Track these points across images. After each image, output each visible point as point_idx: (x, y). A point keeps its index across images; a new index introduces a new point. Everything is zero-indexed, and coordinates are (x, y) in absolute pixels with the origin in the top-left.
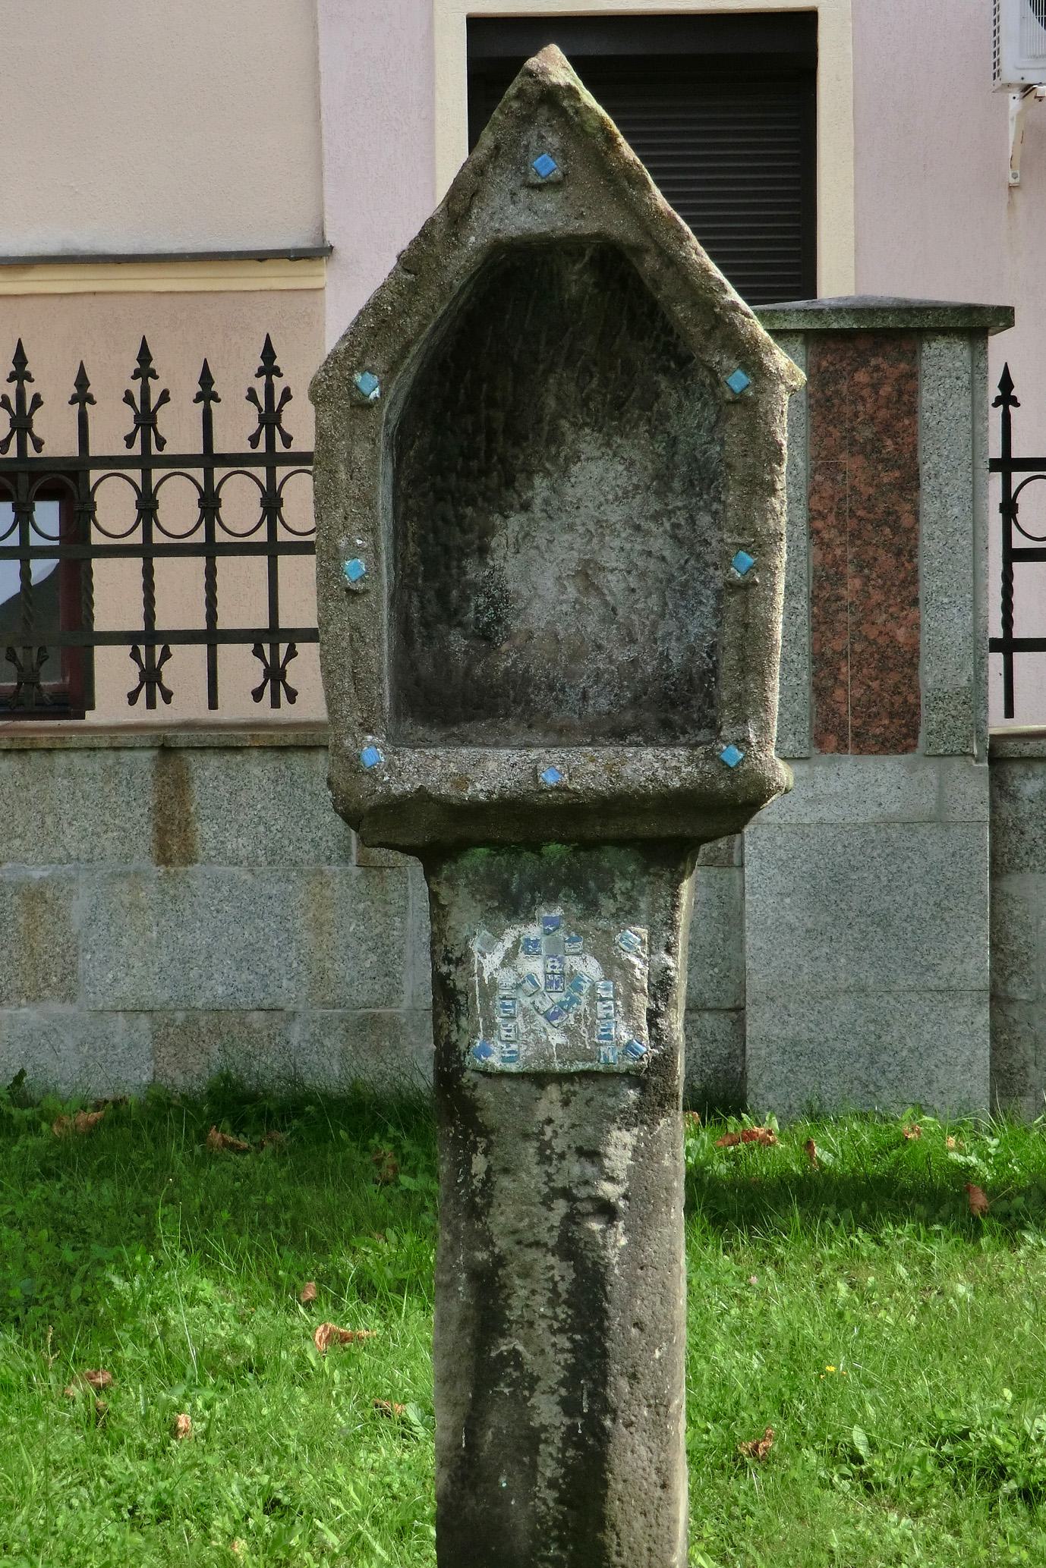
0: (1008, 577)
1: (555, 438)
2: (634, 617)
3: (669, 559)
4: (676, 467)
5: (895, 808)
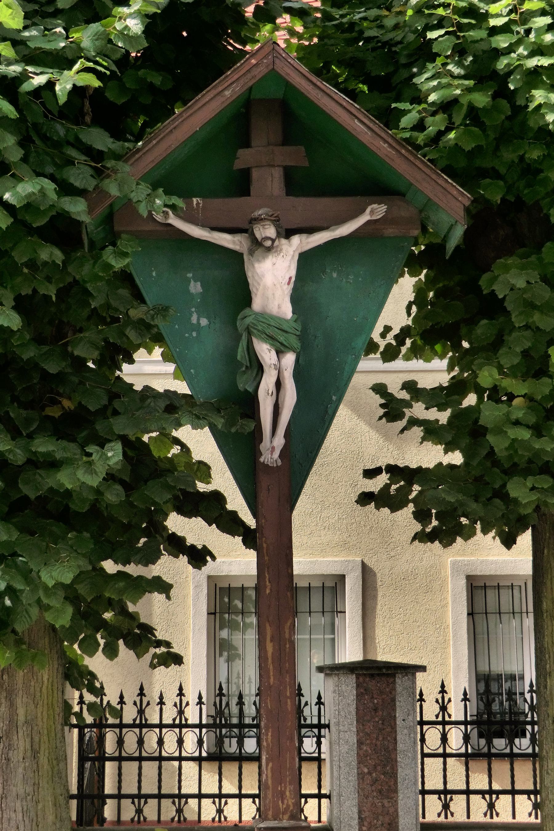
0: (423, 763)
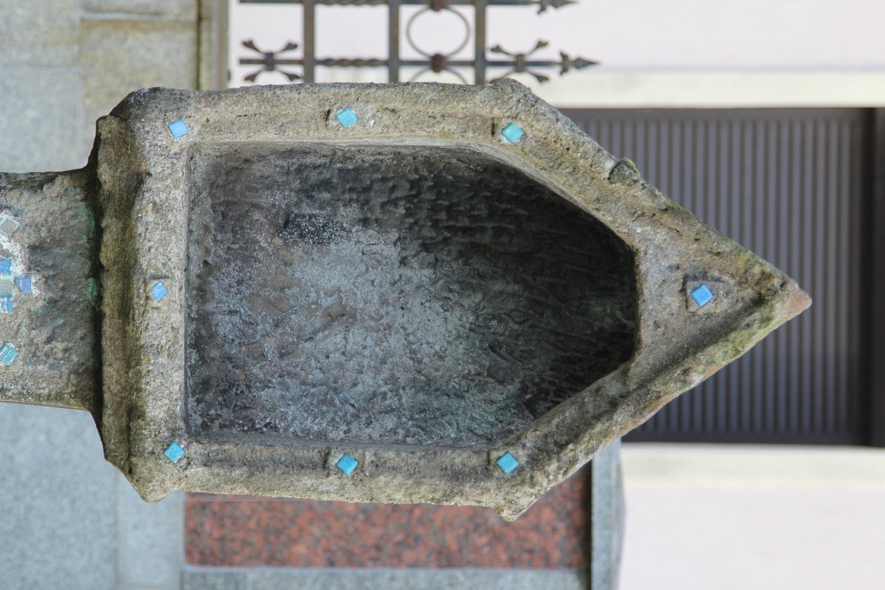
1: (466, 286)
2: (302, 359)
3: (355, 389)
4: (437, 398)
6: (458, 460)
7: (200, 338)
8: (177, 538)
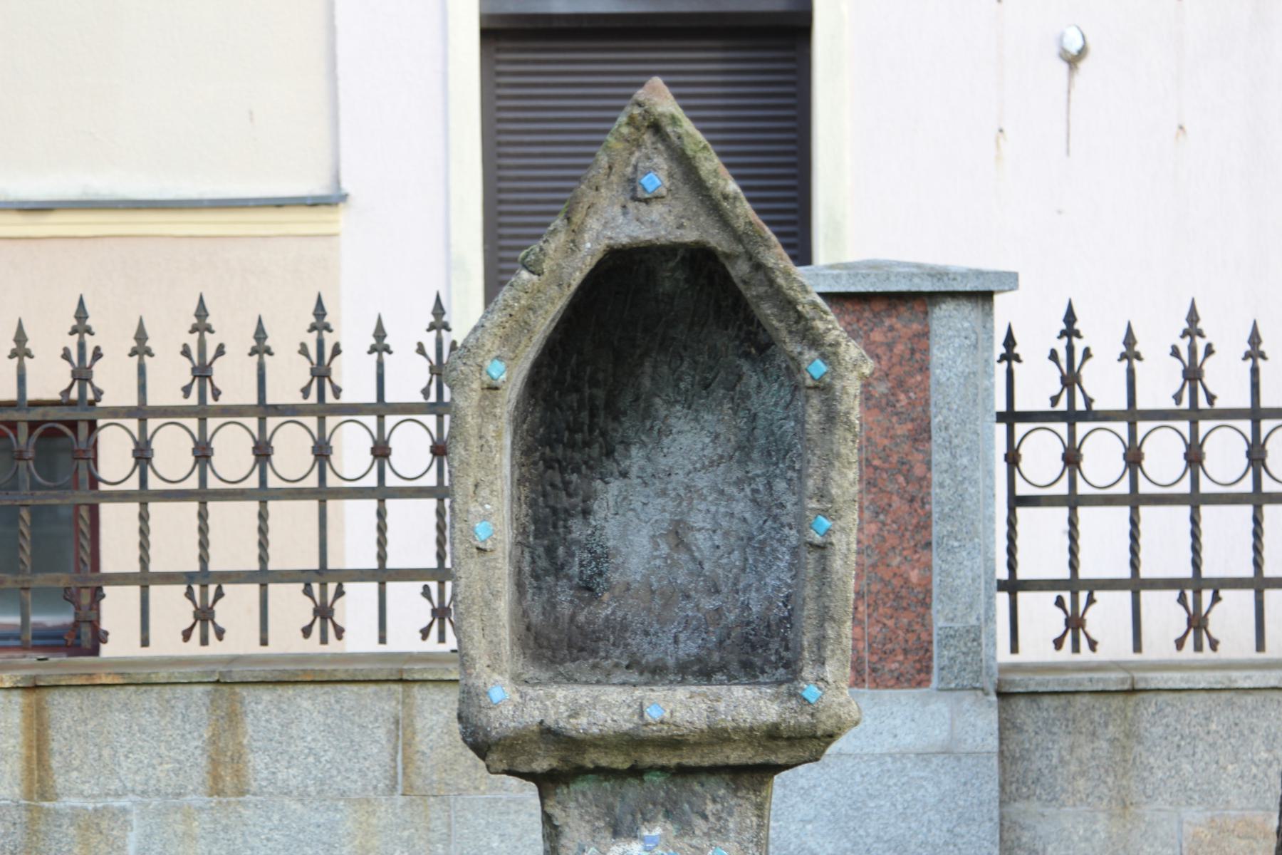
0: (1012, 523)
1: (648, 413)
2: (720, 571)
4: (756, 440)
5: (910, 739)
6: (815, 418)
7: (701, 670)
8: (905, 696)
